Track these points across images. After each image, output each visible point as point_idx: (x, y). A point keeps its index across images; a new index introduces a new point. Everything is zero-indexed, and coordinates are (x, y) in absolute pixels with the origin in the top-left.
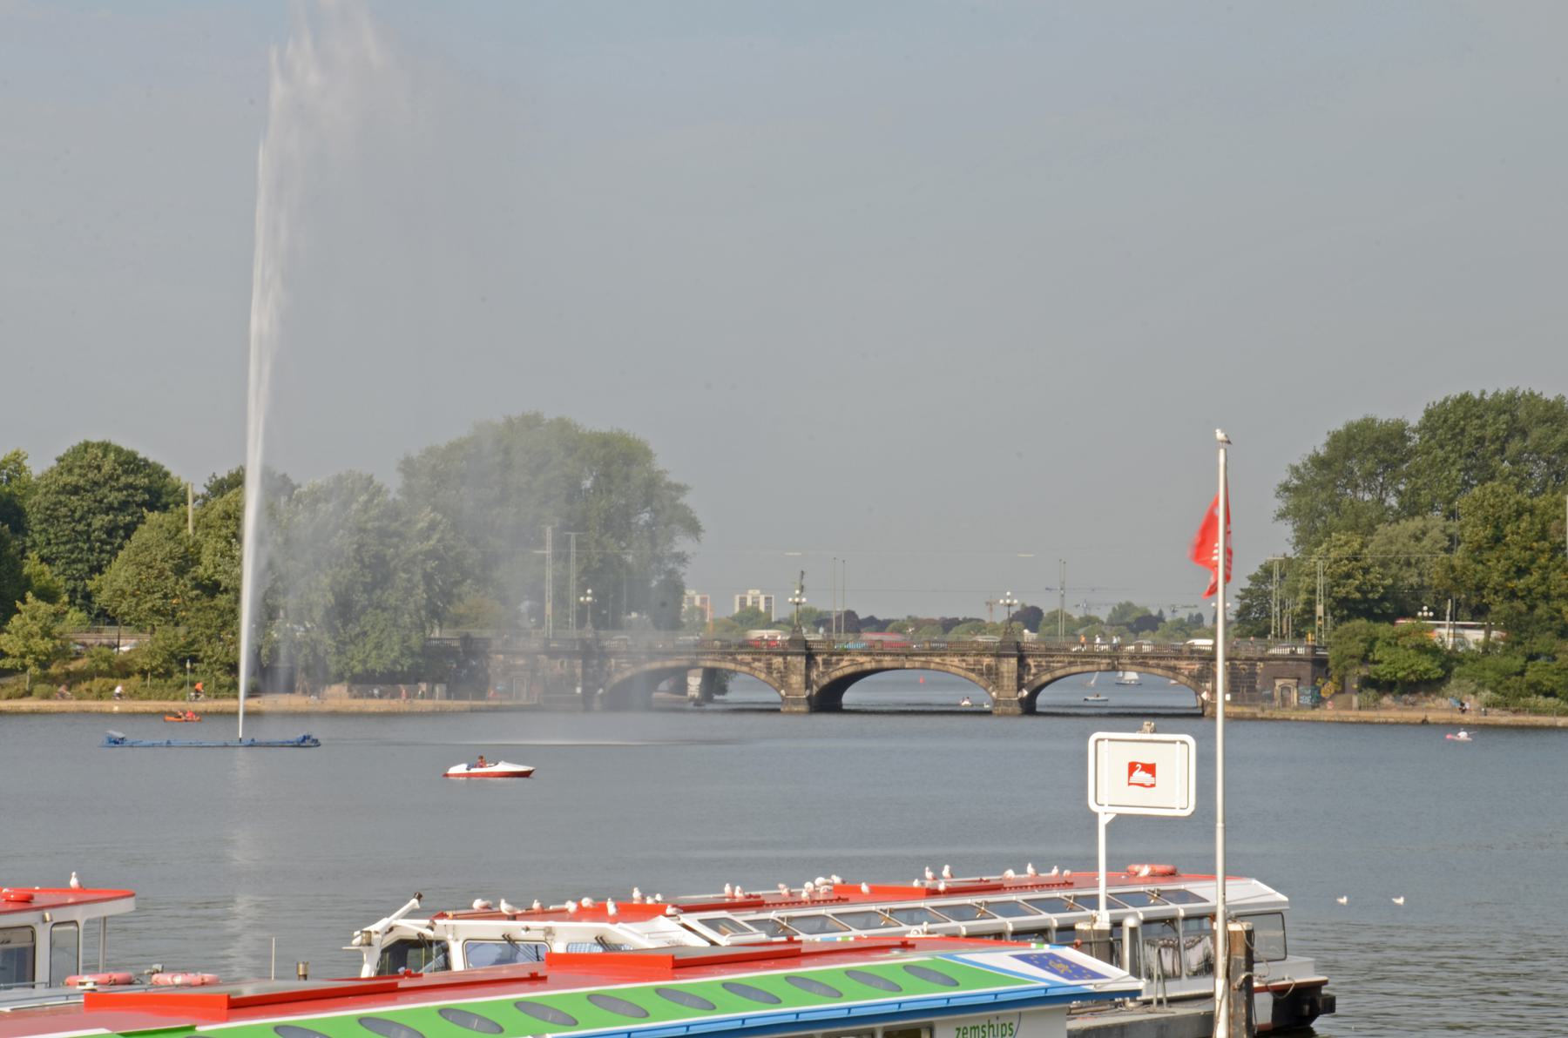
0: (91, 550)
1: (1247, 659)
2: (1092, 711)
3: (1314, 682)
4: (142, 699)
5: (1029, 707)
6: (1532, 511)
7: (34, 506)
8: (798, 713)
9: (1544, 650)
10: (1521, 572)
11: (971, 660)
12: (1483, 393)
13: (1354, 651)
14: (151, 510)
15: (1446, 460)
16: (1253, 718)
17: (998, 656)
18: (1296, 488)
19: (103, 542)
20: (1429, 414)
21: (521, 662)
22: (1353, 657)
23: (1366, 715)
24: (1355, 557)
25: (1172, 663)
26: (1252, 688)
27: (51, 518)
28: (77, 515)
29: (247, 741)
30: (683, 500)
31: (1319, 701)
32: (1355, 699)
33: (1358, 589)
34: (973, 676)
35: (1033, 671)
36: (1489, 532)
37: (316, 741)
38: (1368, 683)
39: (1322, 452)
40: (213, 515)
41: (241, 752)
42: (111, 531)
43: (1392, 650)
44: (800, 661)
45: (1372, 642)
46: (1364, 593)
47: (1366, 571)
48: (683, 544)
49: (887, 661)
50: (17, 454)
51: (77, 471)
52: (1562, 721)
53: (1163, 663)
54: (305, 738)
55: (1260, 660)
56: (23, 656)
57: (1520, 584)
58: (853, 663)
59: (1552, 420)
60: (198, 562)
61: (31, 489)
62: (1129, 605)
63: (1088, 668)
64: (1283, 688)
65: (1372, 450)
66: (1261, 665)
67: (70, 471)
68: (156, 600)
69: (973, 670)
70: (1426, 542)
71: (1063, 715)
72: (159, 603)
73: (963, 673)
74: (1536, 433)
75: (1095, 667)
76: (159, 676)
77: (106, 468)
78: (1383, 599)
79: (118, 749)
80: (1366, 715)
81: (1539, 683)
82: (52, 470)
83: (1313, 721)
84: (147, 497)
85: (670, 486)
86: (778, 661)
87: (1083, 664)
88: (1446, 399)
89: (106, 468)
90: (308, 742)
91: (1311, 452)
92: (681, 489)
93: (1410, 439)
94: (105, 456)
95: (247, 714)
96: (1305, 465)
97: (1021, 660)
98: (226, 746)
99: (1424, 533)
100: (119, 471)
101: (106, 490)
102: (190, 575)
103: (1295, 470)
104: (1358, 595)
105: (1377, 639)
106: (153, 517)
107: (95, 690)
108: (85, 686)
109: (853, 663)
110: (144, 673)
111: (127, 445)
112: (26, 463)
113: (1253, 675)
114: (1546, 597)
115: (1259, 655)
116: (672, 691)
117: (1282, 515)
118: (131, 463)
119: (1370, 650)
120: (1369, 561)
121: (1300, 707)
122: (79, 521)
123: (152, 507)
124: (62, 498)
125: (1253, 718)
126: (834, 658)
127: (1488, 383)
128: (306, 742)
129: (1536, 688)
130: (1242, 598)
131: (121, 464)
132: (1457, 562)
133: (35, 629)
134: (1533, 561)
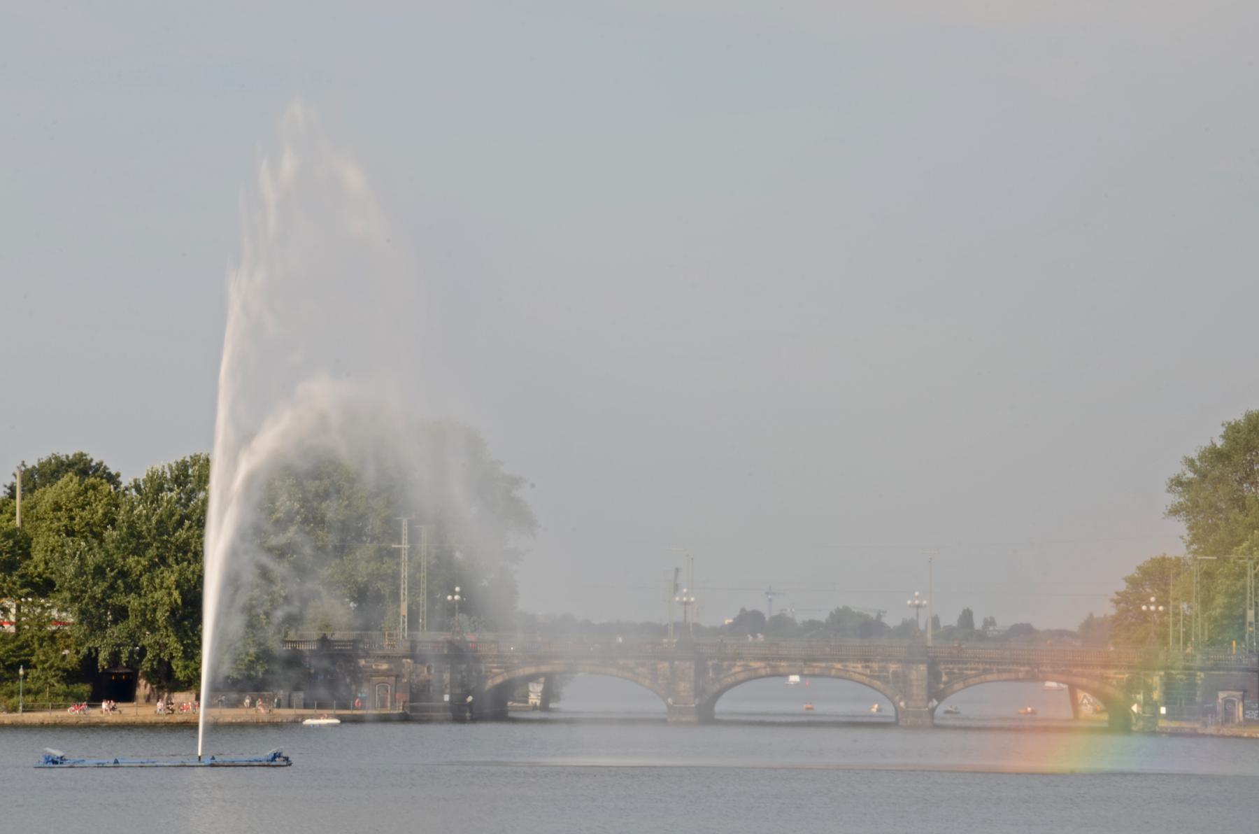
2: (789, 719)
5: (706, 717)
11: (875, 666)
16: (1194, 735)
29: (208, 761)
34: (878, 683)
35: (944, 678)
37: (287, 759)
39: (1220, 443)
40: (42, 508)
54: (275, 756)
60: (28, 556)
64: (1227, 701)
69: (878, 678)
71: (1001, 729)
73: (867, 680)
75: (1013, 675)
79: (56, 772)
86: (664, 666)
87: (999, 671)
91: (1207, 444)
102: (20, 571)
103: (1190, 463)
117: (1175, 511)
125: (1194, 735)
126: (726, 664)
130: (1117, 602)
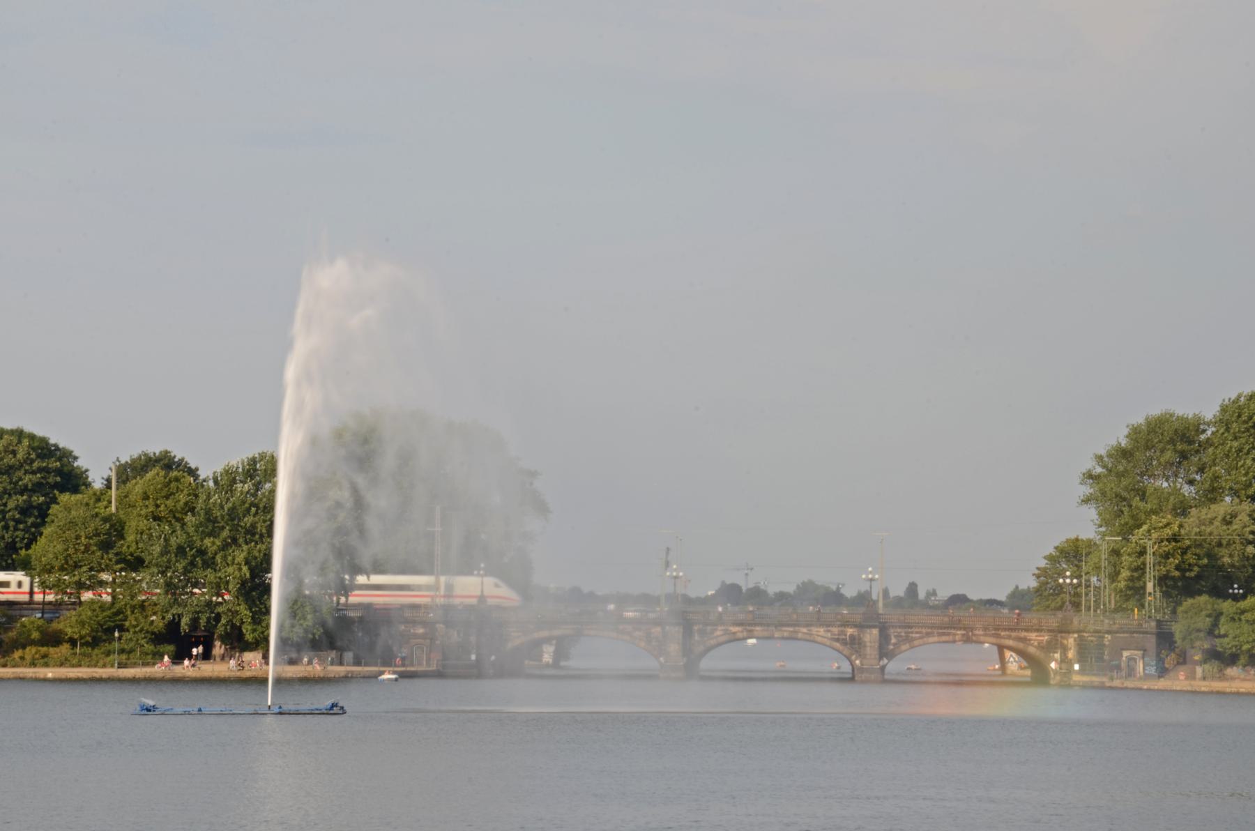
1: (1096, 631)
3: (1158, 654)
4: (73, 666)
13: (1200, 625)
14: (61, 492)
15: (1240, 450)
17: (860, 627)
19: (18, 522)
20: (1224, 409)
22: (1199, 630)
25: (1023, 634)
26: (1100, 658)
31: (1163, 672)
34: (837, 645)
35: (893, 640)
38: (1215, 655)
39: (1124, 443)
41: (269, 719)
42: (25, 511)
44: (676, 631)
45: (1217, 616)
46: (1183, 571)
53: (1014, 634)
54: (333, 706)
55: (1109, 632)
62: (811, 583)
64: (1130, 659)
65: (1172, 441)
66: (1108, 637)
69: (837, 640)
70: (1236, 526)
73: (828, 643)
75: (951, 638)
76: (87, 644)
77: (20, 456)
79: (151, 718)
80: (1218, 685)
83: (1218, 693)
84: (58, 479)
86: (657, 630)
87: (941, 635)
88: (1239, 396)
89: (20, 456)
90: (336, 710)
91: (1114, 443)
93: (1204, 431)
94: (20, 442)
95: (279, 681)
97: (883, 630)
100: (33, 456)
101: (20, 473)
104: (1177, 574)
105: (1221, 614)
106: (65, 498)
107: (28, 658)
108: (17, 654)
110: (73, 642)
111: (39, 432)
113: (1101, 646)
115: (1106, 627)
117: (1086, 501)
118: (44, 449)
119: (1215, 624)
120: (1188, 542)
121: (1147, 677)
123: (63, 489)
126: (709, 628)
128: (335, 710)
130: (1038, 577)
131: (33, 449)
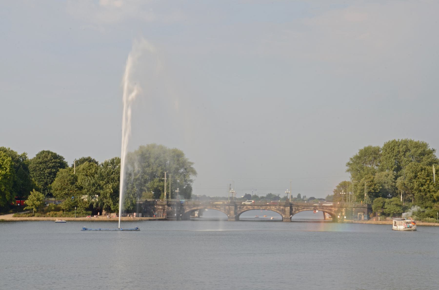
0: (45, 178)
2: (312, 221)
3: (368, 213)
5: (237, 219)
6: (425, 169)
7: (31, 167)
8: (233, 221)
9: (429, 205)
10: (422, 185)
11: (278, 207)
12: (399, 140)
13: (379, 205)
14: (60, 168)
18: (351, 164)
19: (48, 176)
20: (385, 145)
21: (161, 207)
22: (379, 207)
23: (384, 222)
24: (372, 181)
25: (330, 208)
27: (35, 170)
28: (42, 169)
30: (192, 166)
31: (369, 218)
32: (379, 218)
33: (373, 189)
34: (278, 211)
35: (294, 210)
36: (414, 175)
38: (383, 214)
42: (50, 173)
43: (389, 205)
44: (233, 208)
47: (375, 185)
48: (192, 177)
49: (256, 207)
50: (24, 153)
51: (41, 158)
52: (437, 224)
56: (32, 206)
57: (422, 188)
58: (247, 208)
59: (417, 147)
60: (77, 181)
61: (29, 162)
62: (271, 194)
63: (308, 209)
64: (360, 215)
67: (39, 158)
68: (66, 191)
69: (278, 210)
70: (389, 177)
71: (307, 222)
72: (67, 192)
74: (413, 150)
76: (67, 211)
78: (379, 192)
80: (384, 222)
81: (429, 214)
82: (35, 158)
85: (189, 163)
87: (307, 208)
92: (192, 163)
94: (49, 154)
96: (354, 158)
98: (116, 230)
99: (388, 175)
104: (373, 191)
106: (61, 170)
107: (51, 214)
108: (48, 214)
109: (247, 208)
110: (63, 210)
111: (54, 151)
112: (27, 156)
113: (352, 211)
114: (429, 191)
116: (376, 220)
117: (348, 171)
118: (55, 156)
119: (384, 205)
121: (365, 220)
122: (42, 171)
124: (38, 165)
127: (400, 137)
128: (137, 229)
129: (428, 215)
130: (334, 192)
132: (406, 183)
133: (35, 199)
134: (426, 182)
